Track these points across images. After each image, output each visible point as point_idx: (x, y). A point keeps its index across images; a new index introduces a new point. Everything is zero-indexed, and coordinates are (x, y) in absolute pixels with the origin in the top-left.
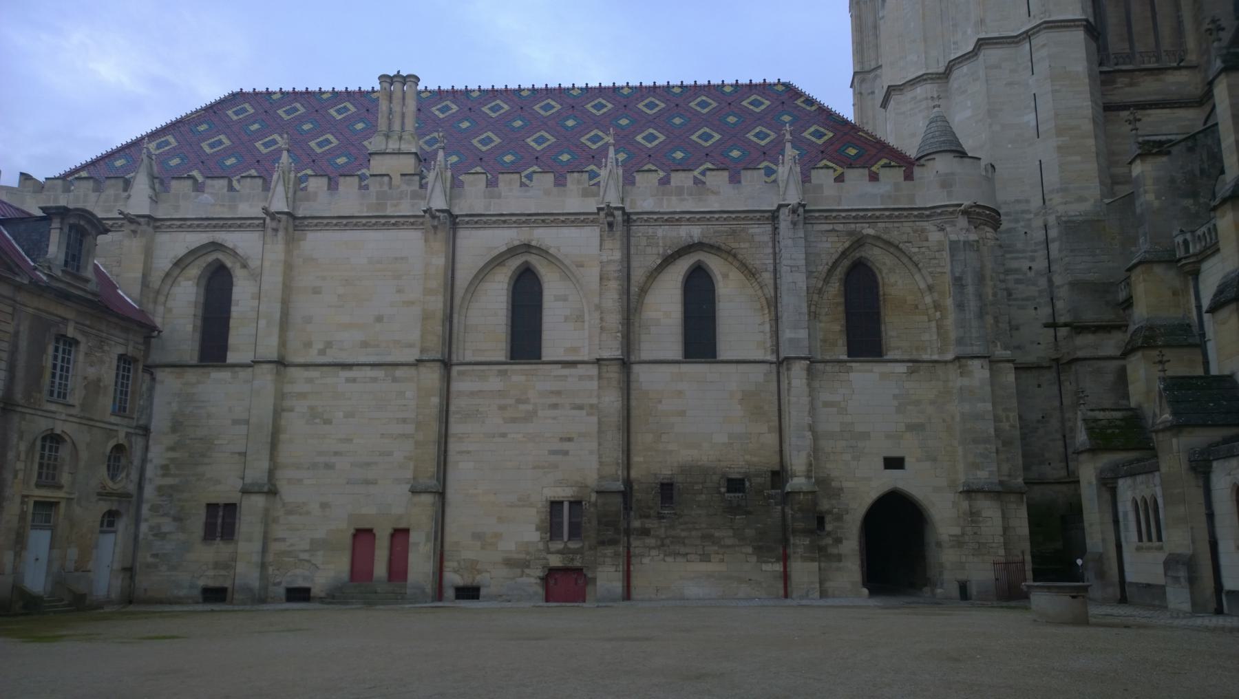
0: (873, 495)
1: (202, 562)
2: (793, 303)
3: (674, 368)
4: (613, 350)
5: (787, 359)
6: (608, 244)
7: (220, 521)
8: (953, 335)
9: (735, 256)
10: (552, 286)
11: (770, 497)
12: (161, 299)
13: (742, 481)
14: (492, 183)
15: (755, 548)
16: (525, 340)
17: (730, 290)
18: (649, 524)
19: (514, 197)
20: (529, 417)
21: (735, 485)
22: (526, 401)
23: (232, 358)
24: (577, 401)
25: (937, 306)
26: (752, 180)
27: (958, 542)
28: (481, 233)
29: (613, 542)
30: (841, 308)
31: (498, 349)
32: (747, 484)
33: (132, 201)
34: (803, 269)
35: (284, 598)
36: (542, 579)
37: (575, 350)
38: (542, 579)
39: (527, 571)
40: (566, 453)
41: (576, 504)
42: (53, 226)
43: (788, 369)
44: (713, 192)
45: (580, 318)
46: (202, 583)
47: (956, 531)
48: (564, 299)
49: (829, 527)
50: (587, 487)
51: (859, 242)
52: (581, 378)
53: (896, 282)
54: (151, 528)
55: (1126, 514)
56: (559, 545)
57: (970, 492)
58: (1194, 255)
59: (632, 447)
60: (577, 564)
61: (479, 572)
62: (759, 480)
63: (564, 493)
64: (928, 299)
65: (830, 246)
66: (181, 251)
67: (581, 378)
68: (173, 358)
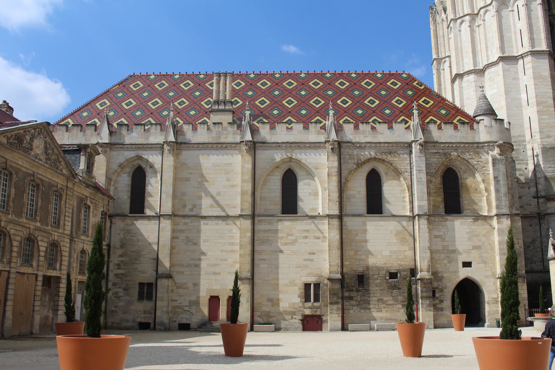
1: (139, 310)
7: (145, 291)
9: (391, 164)
18: (352, 294)
19: (281, 134)
21: (393, 275)
22: (292, 235)
23: (148, 212)
26: (399, 128)
28: (267, 152)
29: (336, 303)
30: (442, 190)
32: (399, 275)
34: (425, 172)
35: (177, 328)
36: (301, 320)
38: (301, 320)
40: (312, 260)
41: (317, 286)
42: (82, 154)
44: (381, 134)
46: (138, 320)
50: (322, 276)
54: (113, 294)
56: (309, 304)
59: (344, 257)
60: (318, 313)
61: (271, 317)
62: (404, 273)
63: (311, 280)
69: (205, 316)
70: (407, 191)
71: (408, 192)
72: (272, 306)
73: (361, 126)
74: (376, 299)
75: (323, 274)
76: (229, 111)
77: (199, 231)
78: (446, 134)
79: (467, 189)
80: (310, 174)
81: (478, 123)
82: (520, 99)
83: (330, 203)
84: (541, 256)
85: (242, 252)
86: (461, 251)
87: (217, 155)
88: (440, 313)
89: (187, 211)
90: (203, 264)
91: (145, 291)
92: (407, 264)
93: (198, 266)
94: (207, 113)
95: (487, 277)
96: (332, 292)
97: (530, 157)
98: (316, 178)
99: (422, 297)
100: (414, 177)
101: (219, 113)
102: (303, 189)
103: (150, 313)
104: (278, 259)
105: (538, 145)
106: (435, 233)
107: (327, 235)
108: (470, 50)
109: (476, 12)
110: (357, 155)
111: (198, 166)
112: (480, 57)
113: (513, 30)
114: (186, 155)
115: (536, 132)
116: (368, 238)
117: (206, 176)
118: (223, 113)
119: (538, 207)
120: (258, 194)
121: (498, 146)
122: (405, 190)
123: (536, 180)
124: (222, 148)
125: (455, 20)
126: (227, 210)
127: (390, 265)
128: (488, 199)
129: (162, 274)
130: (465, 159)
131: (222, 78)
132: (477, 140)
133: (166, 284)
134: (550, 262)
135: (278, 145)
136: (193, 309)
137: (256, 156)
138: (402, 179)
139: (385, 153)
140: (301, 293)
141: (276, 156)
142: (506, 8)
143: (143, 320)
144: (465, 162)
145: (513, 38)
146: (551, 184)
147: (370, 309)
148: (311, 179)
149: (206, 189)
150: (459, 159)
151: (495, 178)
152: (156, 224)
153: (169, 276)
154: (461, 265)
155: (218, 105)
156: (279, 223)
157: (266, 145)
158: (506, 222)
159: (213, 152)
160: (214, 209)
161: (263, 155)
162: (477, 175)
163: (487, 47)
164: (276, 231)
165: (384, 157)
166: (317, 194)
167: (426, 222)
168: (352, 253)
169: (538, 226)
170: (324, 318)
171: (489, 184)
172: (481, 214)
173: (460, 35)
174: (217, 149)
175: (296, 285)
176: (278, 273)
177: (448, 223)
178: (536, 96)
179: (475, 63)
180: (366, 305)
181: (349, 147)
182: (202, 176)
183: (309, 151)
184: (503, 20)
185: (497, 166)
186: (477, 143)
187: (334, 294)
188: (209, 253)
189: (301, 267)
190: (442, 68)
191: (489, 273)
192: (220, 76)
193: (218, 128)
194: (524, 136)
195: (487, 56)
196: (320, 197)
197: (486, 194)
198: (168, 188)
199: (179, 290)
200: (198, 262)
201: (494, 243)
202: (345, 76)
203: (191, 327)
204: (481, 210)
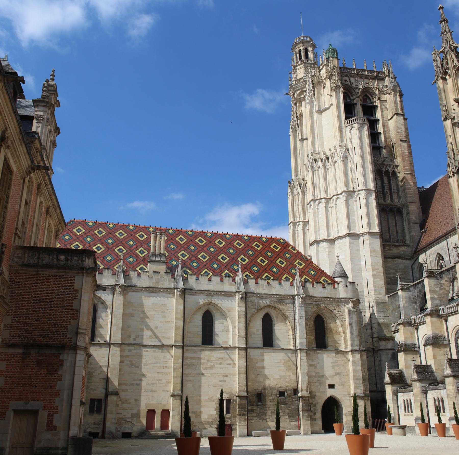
4: (244, 345)
6: (240, 305)
7: (96, 406)
9: (281, 311)
11: (293, 398)
14: (197, 279)
15: (289, 417)
19: (204, 284)
21: (282, 394)
22: (211, 362)
29: (244, 415)
30: (314, 331)
31: (199, 340)
32: (286, 393)
34: (304, 318)
39: (211, 425)
40: (225, 381)
44: (274, 288)
46: (89, 430)
49: (312, 409)
50: (232, 394)
55: (401, 404)
58: (417, 323)
62: (290, 392)
69: (143, 426)
70: (291, 331)
71: (291, 332)
72: (196, 417)
73: (260, 281)
74: (270, 411)
75: (233, 392)
76: (163, 262)
77: (141, 357)
78: (317, 291)
79: (331, 331)
80: (224, 315)
81: (338, 284)
82: (360, 265)
83: (240, 338)
84: (375, 380)
85: (175, 375)
86: (328, 376)
87: (156, 297)
88: (314, 422)
89: (131, 341)
90: (144, 383)
91: (96, 406)
92: (291, 385)
93: (139, 385)
94: (145, 261)
95: (345, 396)
96: (241, 407)
97: (367, 307)
98: (228, 319)
99: (303, 411)
100: (297, 321)
101: (156, 263)
102: (218, 326)
103: (99, 424)
104: (201, 380)
105: (373, 300)
106: (311, 363)
107: (237, 363)
108: (325, 224)
109: (329, 197)
110: (258, 303)
111: (141, 305)
112: (332, 230)
113: (356, 215)
114: (132, 295)
115: (371, 290)
116: (265, 365)
117: (147, 313)
118: (158, 263)
119: (373, 344)
120: (186, 329)
121: (352, 302)
122: (289, 330)
123: (371, 325)
124: (160, 292)
125: (314, 200)
126: (163, 340)
127: (280, 386)
128: (345, 339)
129: (112, 392)
130: (330, 310)
131: (158, 236)
132: (338, 296)
133: (115, 399)
134: (386, 386)
135: (201, 292)
136: (134, 421)
137: (186, 299)
138: (287, 322)
139: (277, 302)
140: (217, 407)
141: (200, 300)
142: (351, 199)
143: (92, 431)
144: (329, 311)
145: (356, 220)
146: (382, 328)
147: (266, 419)
148: (224, 319)
149: (147, 323)
150: (326, 309)
151: (350, 324)
152: (106, 350)
153: (116, 394)
154: (327, 387)
155: (155, 257)
156: (202, 352)
157: (193, 291)
158: (358, 356)
159: (153, 294)
160: (153, 339)
161: (190, 298)
162: (337, 321)
163: (337, 224)
164: (200, 358)
165: (276, 305)
166: (230, 331)
167: (305, 354)
168: (253, 376)
169: (373, 358)
170: (233, 427)
171: (345, 328)
172: (340, 349)
173: (318, 212)
174: (156, 292)
175: (213, 401)
176: (200, 392)
177: (319, 355)
178: (372, 264)
179: (328, 235)
180: (263, 417)
181: (252, 296)
182: (144, 313)
183: (224, 298)
184: (350, 207)
185: (351, 316)
186: (338, 298)
187: (242, 408)
188: (148, 375)
189: (217, 387)
190: (296, 229)
191: (346, 393)
192: (156, 234)
193: (157, 276)
194: (363, 292)
195: (338, 231)
196: (231, 333)
197: (344, 335)
198: (118, 321)
199: (124, 405)
200: (139, 382)
201: (349, 371)
202: (240, 237)
203: (132, 435)
204: (340, 346)
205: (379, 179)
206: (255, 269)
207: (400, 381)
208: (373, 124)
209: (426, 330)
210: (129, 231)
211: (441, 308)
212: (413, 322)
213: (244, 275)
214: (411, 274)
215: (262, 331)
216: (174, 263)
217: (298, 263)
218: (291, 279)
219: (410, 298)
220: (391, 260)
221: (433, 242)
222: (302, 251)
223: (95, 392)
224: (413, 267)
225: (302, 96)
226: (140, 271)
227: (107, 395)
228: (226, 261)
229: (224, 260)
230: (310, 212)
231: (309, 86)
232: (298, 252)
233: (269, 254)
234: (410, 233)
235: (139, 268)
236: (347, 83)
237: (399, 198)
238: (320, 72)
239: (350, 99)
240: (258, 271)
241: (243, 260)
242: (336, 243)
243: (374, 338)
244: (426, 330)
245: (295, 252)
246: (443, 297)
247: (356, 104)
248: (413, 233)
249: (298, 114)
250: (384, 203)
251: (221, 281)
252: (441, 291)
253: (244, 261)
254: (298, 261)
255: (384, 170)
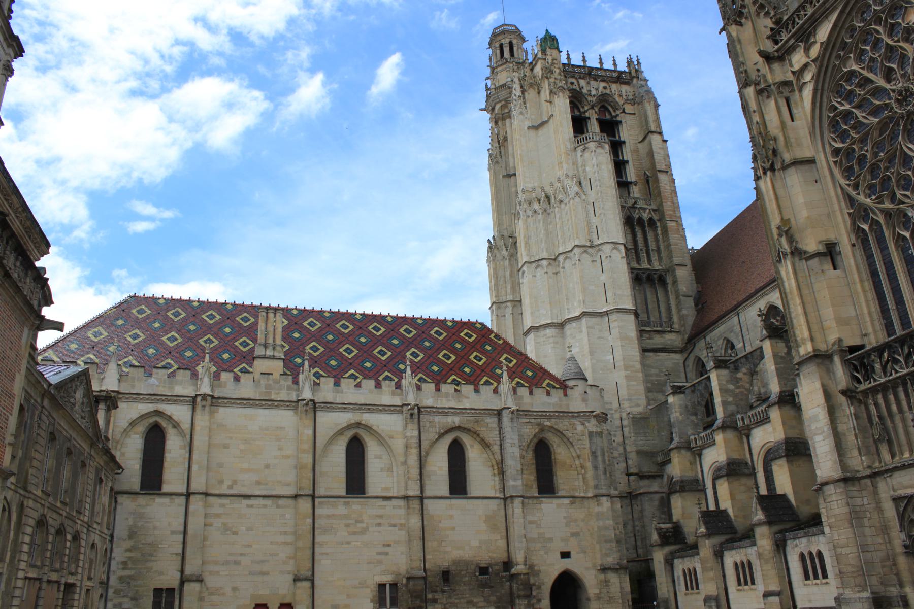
0: (556, 574)
2: (513, 464)
3: (448, 502)
4: (414, 491)
5: (512, 497)
6: (410, 426)
8: (592, 483)
9: (478, 435)
10: (372, 450)
11: (503, 577)
12: (119, 446)
13: (487, 568)
16: (356, 482)
17: (474, 456)
18: (437, 596)
19: (349, 392)
20: (364, 531)
21: (484, 571)
22: (362, 522)
23: (166, 488)
24: (393, 522)
25: (582, 467)
27: (598, 597)
30: (534, 466)
33: (105, 381)
37: (387, 489)
40: (387, 554)
41: (394, 585)
42: (100, 407)
43: (512, 503)
45: (390, 470)
47: (597, 591)
48: (380, 457)
49: (534, 593)
51: (542, 429)
52: (394, 507)
53: (560, 453)
55: (679, 577)
57: (604, 570)
62: (497, 568)
63: (387, 579)
64: (577, 462)
65: (529, 431)
66: (134, 415)
67: (394, 507)
68: (125, 487)
95: (587, 569)
106: (530, 518)
132: (572, 410)
140: (374, 597)
168: (435, 544)
175: (367, 587)
178: (624, 359)
193: (268, 380)
199: (215, 598)
205: (629, 232)
206: (435, 368)
207: (674, 537)
208: (616, 147)
209: (716, 455)
210: (225, 312)
211: (739, 416)
212: (693, 445)
213: (417, 378)
214: (683, 375)
215: (447, 469)
216: (298, 360)
217: (506, 359)
218: (495, 384)
219: (686, 407)
220: (651, 354)
221: (717, 322)
222: (511, 340)
223: (162, 577)
224: (687, 363)
225: (506, 111)
226: (239, 374)
227: (182, 582)
228: (386, 357)
229: (383, 355)
230: (526, 281)
231: (517, 91)
232: (505, 342)
233: (458, 346)
234: (679, 310)
235: (239, 368)
236: (574, 87)
237: (660, 259)
238: (532, 70)
239: (579, 111)
240: (439, 372)
241: (415, 355)
242: (567, 327)
243: (632, 474)
244: (716, 455)
245: (501, 342)
246: (742, 400)
247: (589, 118)
248: (684, 312)
249: (501, 138)
250: (638, 267)
251: (376, 387)
252: (737, 391)
253: (416, 357)
254: (505, 356)
255: (636, 216)
